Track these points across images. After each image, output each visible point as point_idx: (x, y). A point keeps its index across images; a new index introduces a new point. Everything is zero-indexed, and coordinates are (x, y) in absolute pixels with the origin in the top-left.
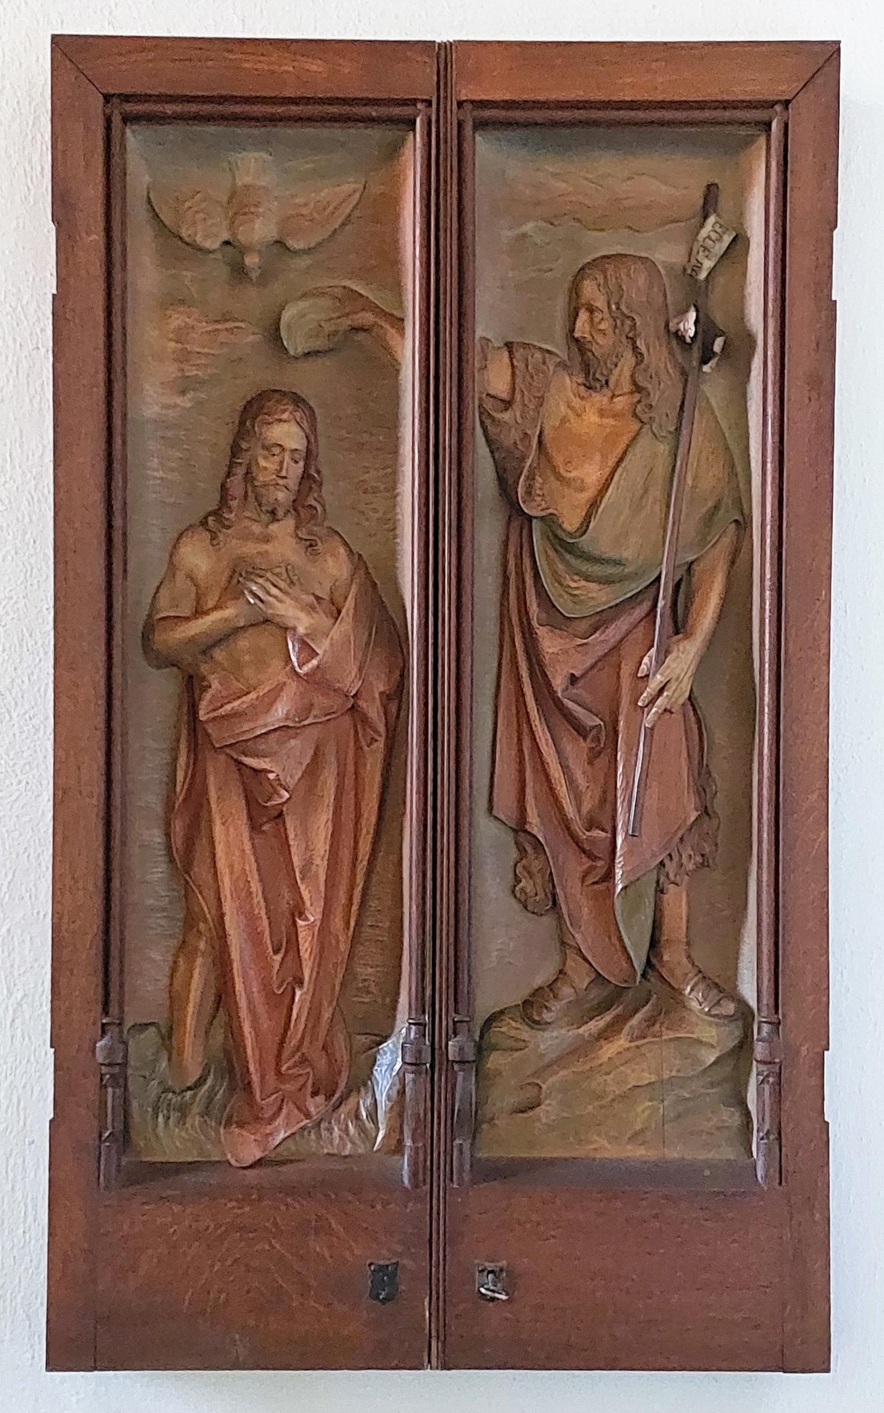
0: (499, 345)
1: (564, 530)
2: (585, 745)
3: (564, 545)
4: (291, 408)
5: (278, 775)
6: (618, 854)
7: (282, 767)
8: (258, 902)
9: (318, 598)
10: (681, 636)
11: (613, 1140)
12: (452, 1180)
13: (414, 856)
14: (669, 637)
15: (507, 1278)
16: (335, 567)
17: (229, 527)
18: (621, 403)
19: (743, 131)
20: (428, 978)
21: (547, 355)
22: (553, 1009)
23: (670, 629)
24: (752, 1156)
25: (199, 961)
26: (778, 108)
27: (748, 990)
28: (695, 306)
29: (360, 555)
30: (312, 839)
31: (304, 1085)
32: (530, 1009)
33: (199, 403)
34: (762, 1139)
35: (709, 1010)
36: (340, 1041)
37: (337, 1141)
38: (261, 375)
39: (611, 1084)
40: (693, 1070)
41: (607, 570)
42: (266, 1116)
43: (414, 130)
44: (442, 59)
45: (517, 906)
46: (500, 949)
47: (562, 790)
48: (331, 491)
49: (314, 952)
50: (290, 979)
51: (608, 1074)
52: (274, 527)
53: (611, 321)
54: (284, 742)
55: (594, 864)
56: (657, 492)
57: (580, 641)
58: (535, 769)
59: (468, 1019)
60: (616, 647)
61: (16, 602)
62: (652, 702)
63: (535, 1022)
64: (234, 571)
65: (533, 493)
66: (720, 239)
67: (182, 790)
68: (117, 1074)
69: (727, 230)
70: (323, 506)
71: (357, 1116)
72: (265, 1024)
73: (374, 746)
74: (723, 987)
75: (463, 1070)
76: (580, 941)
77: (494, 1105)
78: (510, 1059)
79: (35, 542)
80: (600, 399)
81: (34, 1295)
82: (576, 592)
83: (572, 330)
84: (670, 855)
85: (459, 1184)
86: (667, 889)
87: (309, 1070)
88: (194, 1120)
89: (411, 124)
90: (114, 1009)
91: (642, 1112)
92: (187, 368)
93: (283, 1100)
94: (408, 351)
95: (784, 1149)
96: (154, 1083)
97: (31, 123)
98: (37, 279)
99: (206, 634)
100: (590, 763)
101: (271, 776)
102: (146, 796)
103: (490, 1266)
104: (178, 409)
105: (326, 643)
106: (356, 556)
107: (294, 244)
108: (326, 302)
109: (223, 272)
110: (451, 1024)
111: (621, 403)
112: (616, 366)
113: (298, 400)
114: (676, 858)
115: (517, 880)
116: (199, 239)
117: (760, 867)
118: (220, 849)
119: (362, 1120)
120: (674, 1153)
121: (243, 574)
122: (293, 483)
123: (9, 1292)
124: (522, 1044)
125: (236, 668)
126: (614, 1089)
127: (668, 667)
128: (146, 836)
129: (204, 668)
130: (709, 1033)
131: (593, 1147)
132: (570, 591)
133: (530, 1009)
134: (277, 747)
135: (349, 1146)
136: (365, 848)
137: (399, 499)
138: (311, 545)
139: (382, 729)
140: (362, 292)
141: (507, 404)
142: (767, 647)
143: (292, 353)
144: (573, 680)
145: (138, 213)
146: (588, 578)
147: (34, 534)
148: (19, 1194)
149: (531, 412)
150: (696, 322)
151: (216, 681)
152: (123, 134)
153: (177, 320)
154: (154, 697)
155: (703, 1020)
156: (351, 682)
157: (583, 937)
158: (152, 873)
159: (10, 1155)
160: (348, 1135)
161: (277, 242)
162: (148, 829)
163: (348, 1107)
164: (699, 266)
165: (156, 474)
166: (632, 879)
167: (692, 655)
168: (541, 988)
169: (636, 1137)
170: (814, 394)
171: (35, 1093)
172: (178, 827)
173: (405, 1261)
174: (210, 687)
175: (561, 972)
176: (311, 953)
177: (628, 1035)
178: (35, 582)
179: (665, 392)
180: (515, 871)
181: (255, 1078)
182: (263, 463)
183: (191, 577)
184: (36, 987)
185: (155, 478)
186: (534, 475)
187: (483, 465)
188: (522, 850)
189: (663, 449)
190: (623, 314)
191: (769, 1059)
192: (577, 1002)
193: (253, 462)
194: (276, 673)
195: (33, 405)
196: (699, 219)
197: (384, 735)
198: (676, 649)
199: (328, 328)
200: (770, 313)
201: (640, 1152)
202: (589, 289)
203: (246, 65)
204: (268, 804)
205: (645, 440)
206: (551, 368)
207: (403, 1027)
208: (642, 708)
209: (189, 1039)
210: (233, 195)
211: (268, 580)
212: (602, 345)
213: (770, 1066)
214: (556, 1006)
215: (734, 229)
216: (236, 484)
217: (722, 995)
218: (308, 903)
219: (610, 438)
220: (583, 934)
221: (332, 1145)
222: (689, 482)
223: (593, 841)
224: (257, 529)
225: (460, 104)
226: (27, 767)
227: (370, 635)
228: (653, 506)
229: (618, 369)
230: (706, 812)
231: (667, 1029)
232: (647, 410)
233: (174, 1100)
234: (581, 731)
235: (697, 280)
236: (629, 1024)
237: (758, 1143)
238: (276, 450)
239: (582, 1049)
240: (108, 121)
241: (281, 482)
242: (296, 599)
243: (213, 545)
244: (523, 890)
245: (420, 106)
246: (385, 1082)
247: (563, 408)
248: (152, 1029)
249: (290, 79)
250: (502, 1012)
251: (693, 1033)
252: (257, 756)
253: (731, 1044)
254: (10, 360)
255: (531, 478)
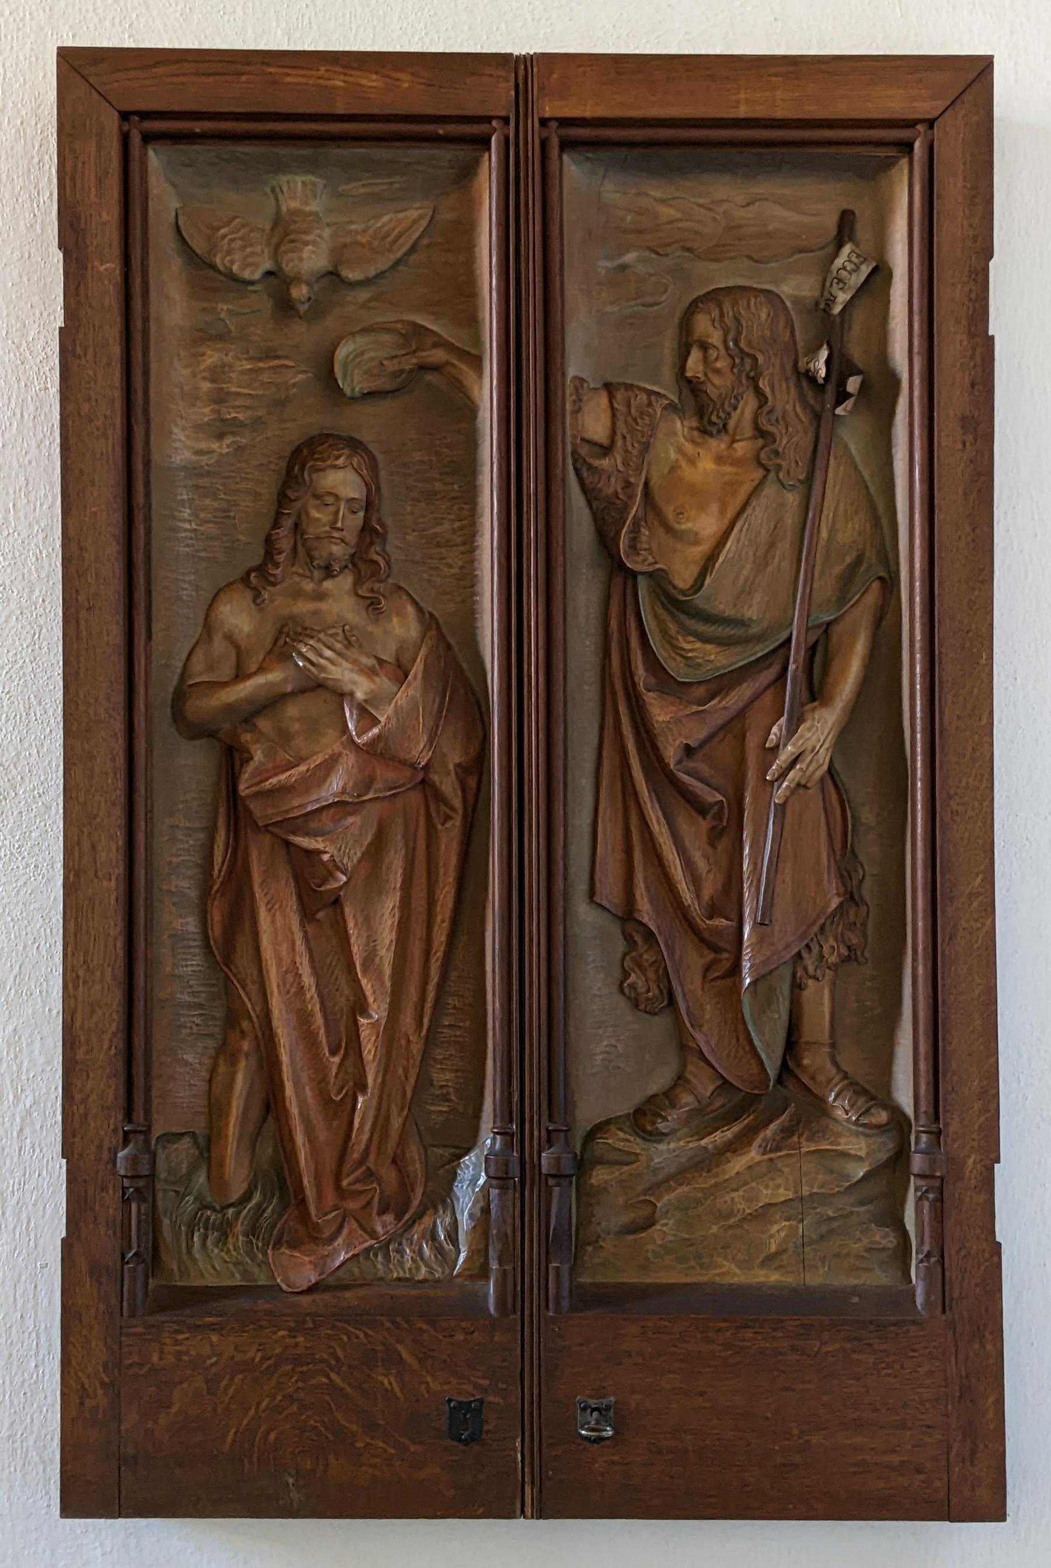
0: (597, 386)
1: (675, 587)
2: (705, 825)
3: (675, 604)
4: (346, 451)
5: (332, 856)
6: (745, 944)
7: (339, 848)
8: (312, 998)
9: (381, 662)
10: (816, 704)
11: (745, 1265)
12: (547, 1307)
13: (497, 946)
14: (803, 705)
15: (614, 1414)
16: (402, 627)
17: (274, 584)
18: (742, 448)
19: (882, 153)
20: (515, 1082)
21: (653, 398)
22: (669, 1118)
23: (805, 695)
24: (911, 1281)
25: (242, 1063)
26: (920, 128)
27: (904, 1096)
28: (828, 343)
29: (431, 615)
30: (377, 930)
31: (369, 1203)
32: (643, 1120)
33: (239, 449)
34: (921, 1261)
35: (857, 1119)
36: (414, 1151)
37: (409, 1264)
38: (310, 418)
39: (738, 1201)
40: (838, 1186)
41: (728, 630)
42: (326, 1236)
43: (489, 149)
44: (521, 72)
45: (623, 1004)
46: (606, 1052)
47: (677, 872)
48: (396, 546)
49: (378, 1053)
50: (351, 1084)
51: (736, 1190)
52: (328, 584)
53: (729, 361)
54: (340, 820)
55: (718, 956)
56: (785, 546)
57: (695, 708)
58: (645, 852)
59: (564, 1128)
60: (741, 714)
61: (21, 667)
62: (783, 775)
63: (651, 1133)
64: (281, 632)
65: (638, 546)
66: (857, 269)
67: (220, 871)
68: (142, 1187)
69: (865, 260)
70: (388, 563)
71: (433, 1236)
72: (322, 1135)
73: (448, 825)
74: (874, 1092)
75: (558, 1185)
76: (702, 1045)
77: (599, 1224)
78: (617, 1174)
79: (43, 601)
80: (718, 445)
81: (48, 1437)
82: (690, 655)
83: (683, 368)
84: (808, 946)
85: (555, 1312)
86: (806, 985)
87: (374, 1185)
88: (238, 1238)
89: (486, 143)
90: (139, 1114)
91: (778, 1233)
92: (224, 410)
93: (344, 1220)
94: (487, 393)
95: (947, 1274)
96: (190, 1199)
97: (37, 146)
98: (45, 314)
99: (248, 700)
100: (712, 843)
101: (326, 857)
102: (177, 880)
103: (593, 1403)
104: (215, 455)
105: (390, 710)
106: (427, 615)
107: (352, 274)
108: (388, 338)
109: (262, 302)
110: (544, 1134)
111: (742, 448)
112: (735, 408)
113: (355, 445)
114: (815, 950)
115: (626, 975)
116: (235, 268)
117: (915, 960)
118: (265, 939)
119: (440, 1243)
120: (817, 1278)
121: (291, 633)
122: (351, 535)
123: (20, 1433)
124: (633, 1158)
125: (285, 737)
126: (744, 1207)
127: (802, 736)
128: (178, 922)
129: (246, 737)
130: (859, 1146)
131: (717, 1271)
132: (684, 653)
133: (643, 1120)
134: (331, 825)
135: (424, 1269)
136: (440, 938)
137: (477, 553)
138: (371, 604)
139: (458, 803)
140: (429, 326)
141: (606, 450)
142: (918, 715)
143: (348, 391)
144: (689, 751)
145: (162, 239)
146: (706, 640)
147: (44, 592)
148: (30, 1323)
149: (634, 459)
150: (828, 362)
151: (259, 752)
152: (144, 156)
153: (212, 357)
154: (185, 773)
155: (850, 1130)
156: (419, 751)
157: (705, 1038)
158: (186, 966)
159: (19, 1281)
160: (422, 1259)
161: (331, 273)
162: (181, 916)
163: (422, 1226)
164: (831, 301)
165: (187, 526)
166: (762, 972)
167: (830, 724)
168: (655, 1096)
169: (770, 1260)
170: (970, 438)
171: (49, 1212)
172: (217, 916)
173: (491, 1398)
174: (252, 758)
175: (679, 1078)
176: (375, 1055)
177: (760, 1146)
178: (45, 643)
179: (793, 440)
180: (623, 966)
181: (310, 1193)
182: (315, 514)
183: (229, 638)
184: (48, 1093)
185: (186, 530)
186: (639, 526)
187: (577, 517)
188: (628, 938)
189: (793, 499)
190: (742, 351)
191: (928, 1173)
192: (698, 1111)
193: (303, 513)
194: (330, 743)
195: (41, 452)
196: (830, 249)
197: (460, 811)
198: (810, 717)
199: (390, 366)
200: (916, 349)
201: (774, 1277)
202: (704, 325)
203: (289, 79)
204: (322, 889)
205: (770, 490)
206: (659, 413)
207: (488, 1140)
208: (772, 782)
209: (231, 1149)
210: (276, 223)
211: (319, 640)
212: (718, 385)
213: (929, 1181)
214: (674, 1115)
215: (874, 259)
216: (284, 540)
217: (872, 1103)
218: (371, 1000)
219: (732, 486)
220: (706, 1036)
221: (403, 1269)
222: (824, 534)
223: (717, 931)
224: (308, 586)
225: (544, 122)
226: (36, 849)
227: (442, 704)
228: (781, 559)
229: (738, 411)
230: (851, 898)
231: (807, 1140)
232: (772, 456)
233: (213, 1217)
234: (700, 808)
235: (830, 315)
236: (761, 1135)
237: (917, 1267)
238: (330, 500)
239: (707, 1162)
240: (125, 140)
241: (336, 534)
242: (354, 662)
243: (257, 605)
244: (633, 986)
245: (494, 123)
246: (467, 1200)
247: (673, 455)
248: (187, 1141)
249: (341, 94)
250: (608, 1122)
251: (838, 1144)
252: (308, 834)
253: (883, 1156)
254: (13, 402)
255: (636, 529)
